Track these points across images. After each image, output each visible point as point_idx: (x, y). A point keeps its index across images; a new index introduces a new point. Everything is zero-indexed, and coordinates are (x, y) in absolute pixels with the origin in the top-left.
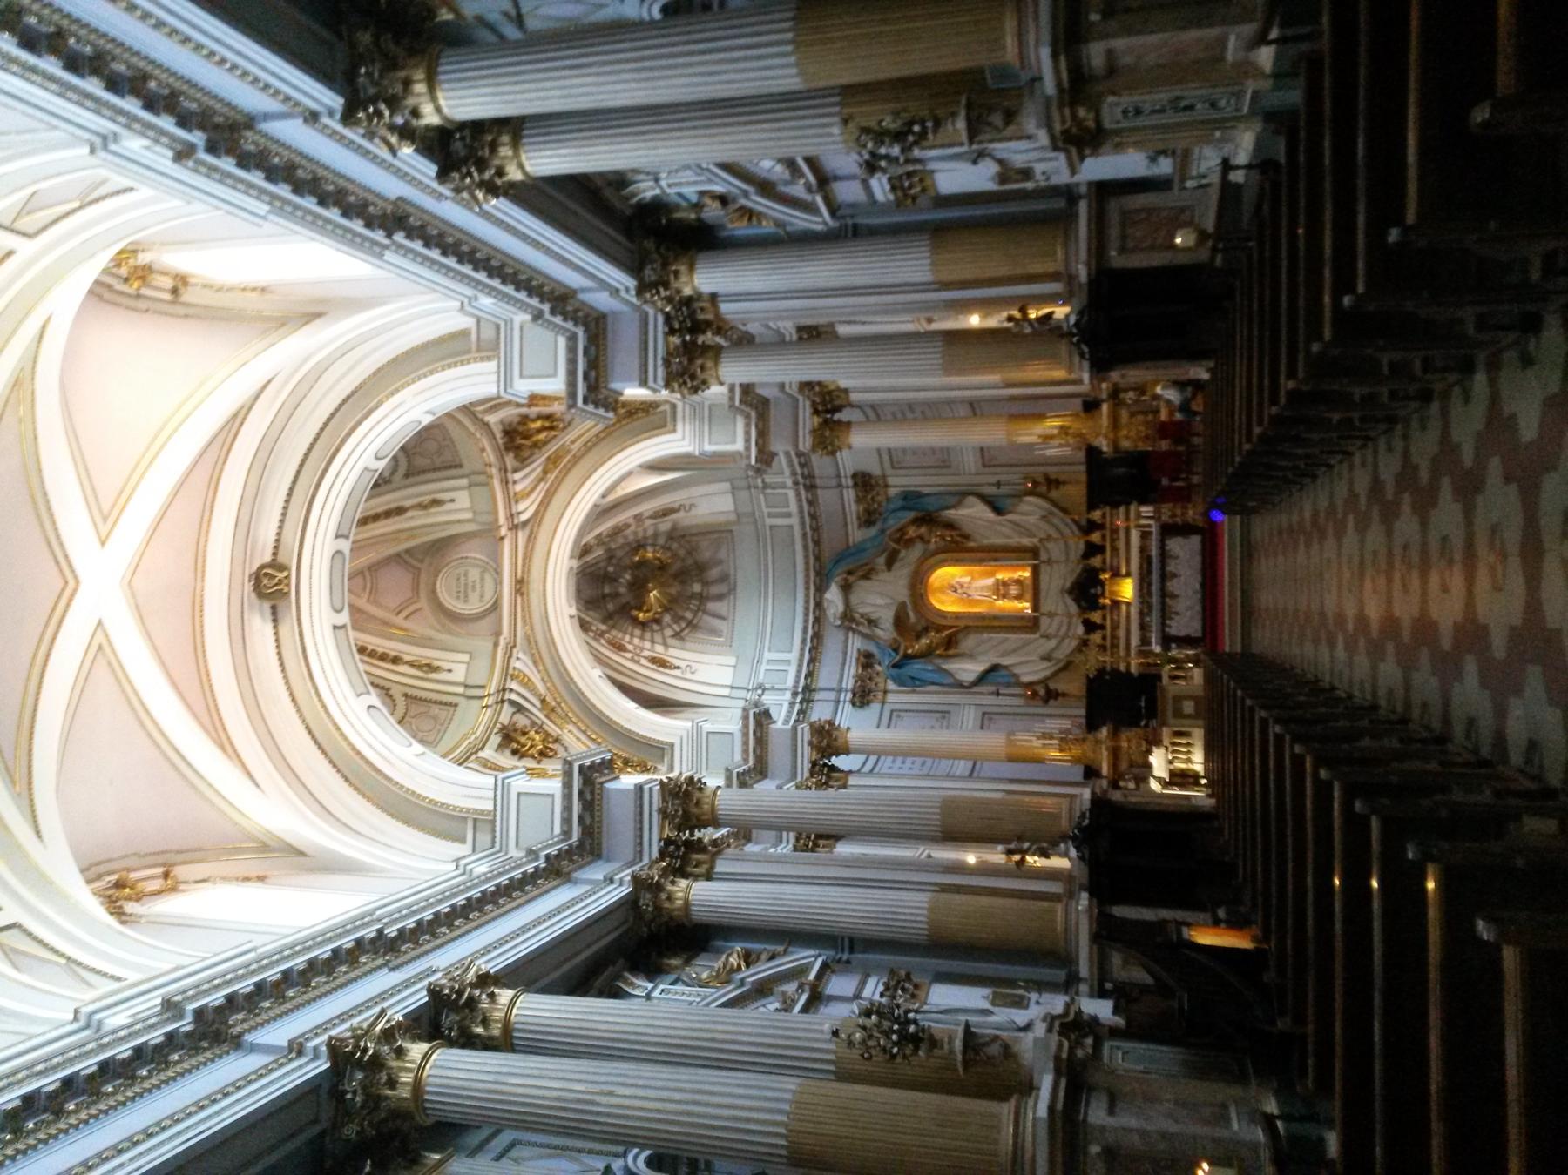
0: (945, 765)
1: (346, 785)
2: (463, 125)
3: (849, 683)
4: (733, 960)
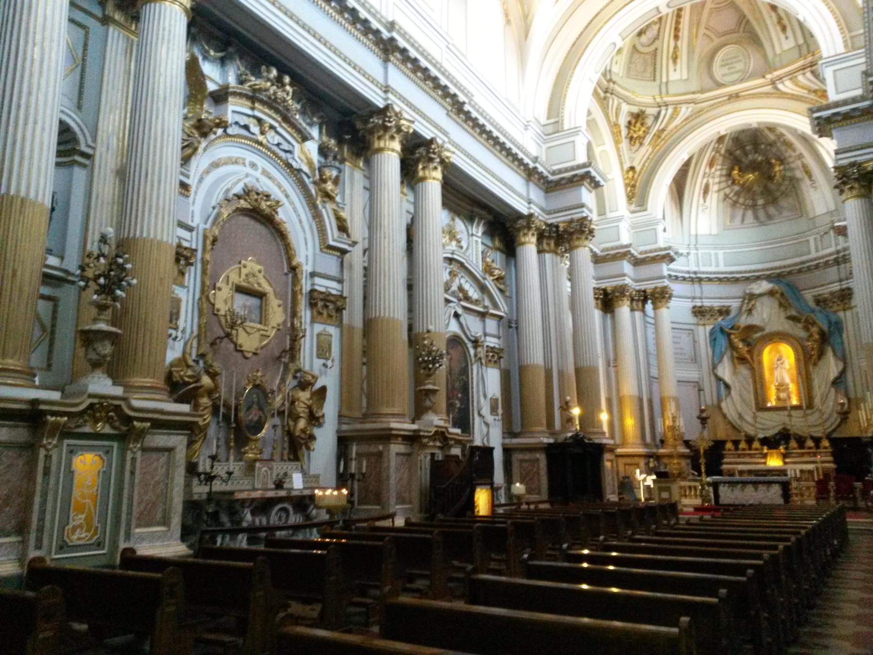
0: (653, 362)
1: (570, 45)
3: (707, 303)
4: (496, 272)
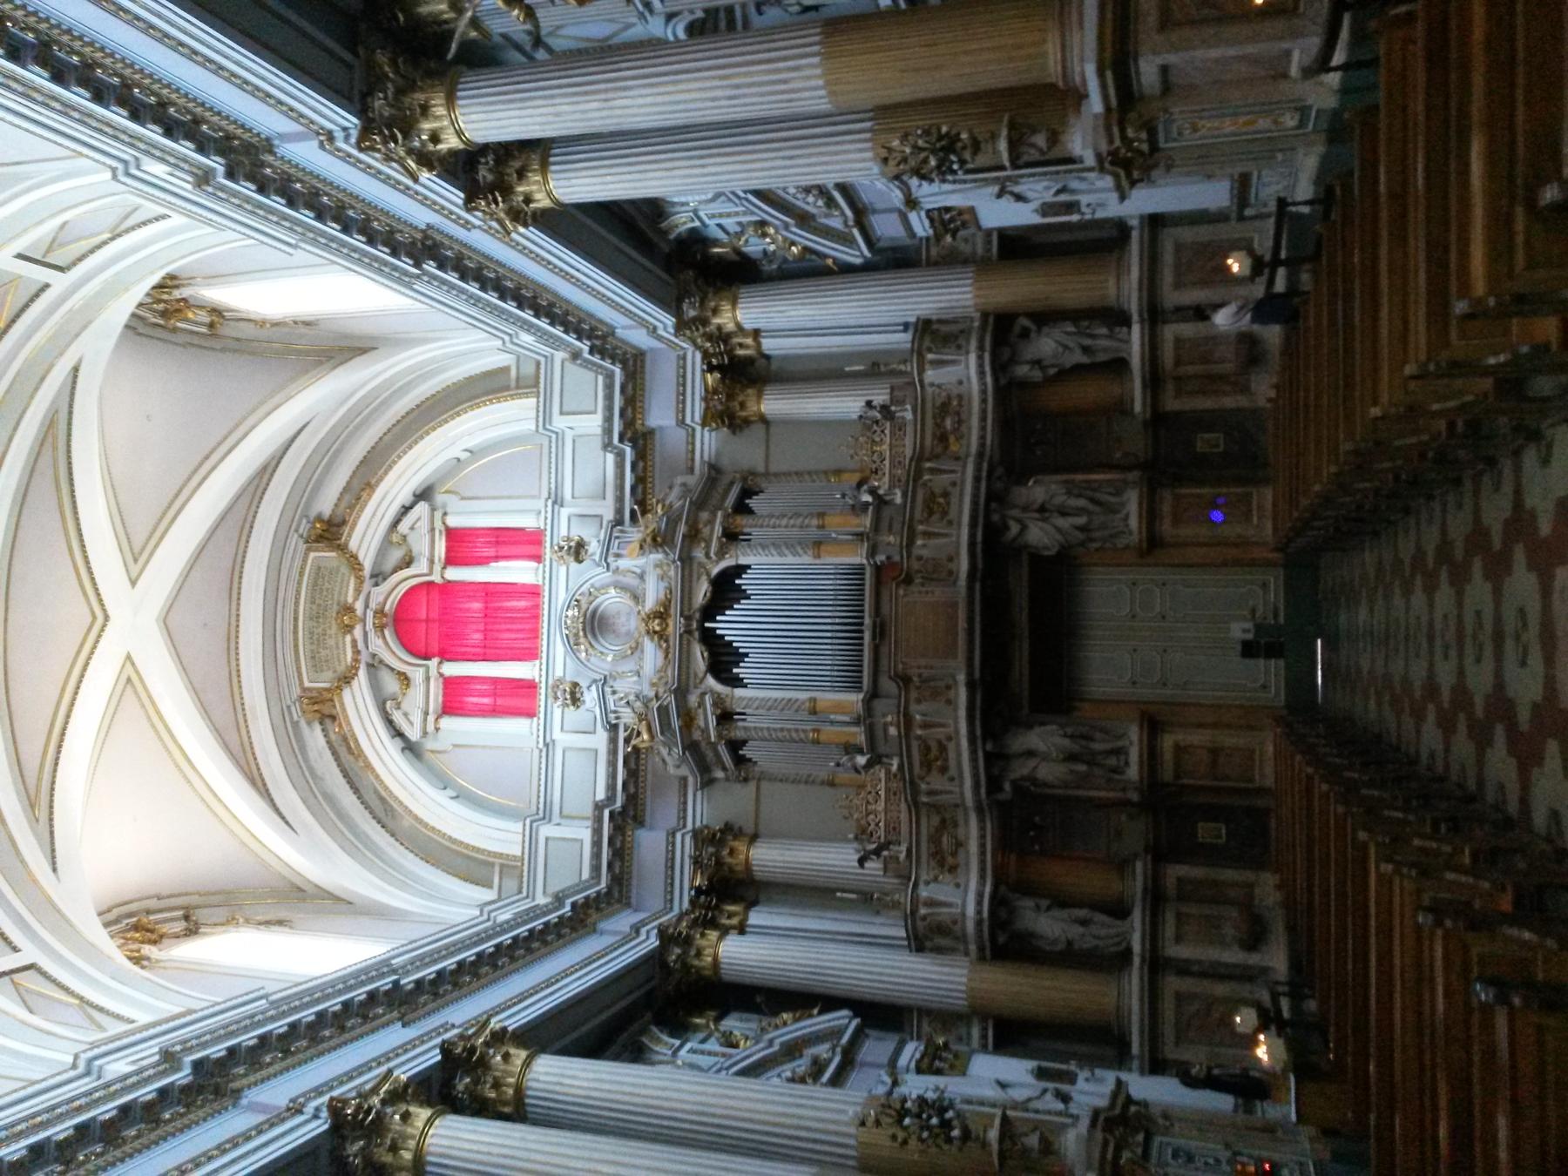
2: (485, 149)
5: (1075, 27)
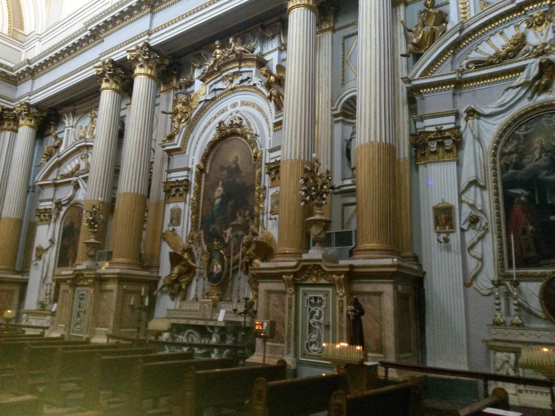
5: (127, 267)
